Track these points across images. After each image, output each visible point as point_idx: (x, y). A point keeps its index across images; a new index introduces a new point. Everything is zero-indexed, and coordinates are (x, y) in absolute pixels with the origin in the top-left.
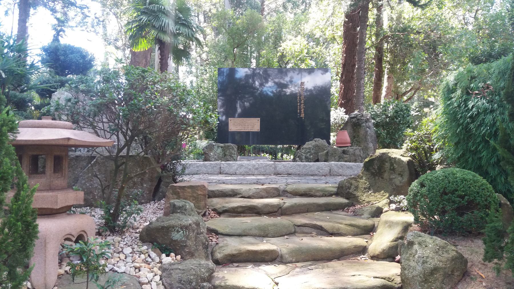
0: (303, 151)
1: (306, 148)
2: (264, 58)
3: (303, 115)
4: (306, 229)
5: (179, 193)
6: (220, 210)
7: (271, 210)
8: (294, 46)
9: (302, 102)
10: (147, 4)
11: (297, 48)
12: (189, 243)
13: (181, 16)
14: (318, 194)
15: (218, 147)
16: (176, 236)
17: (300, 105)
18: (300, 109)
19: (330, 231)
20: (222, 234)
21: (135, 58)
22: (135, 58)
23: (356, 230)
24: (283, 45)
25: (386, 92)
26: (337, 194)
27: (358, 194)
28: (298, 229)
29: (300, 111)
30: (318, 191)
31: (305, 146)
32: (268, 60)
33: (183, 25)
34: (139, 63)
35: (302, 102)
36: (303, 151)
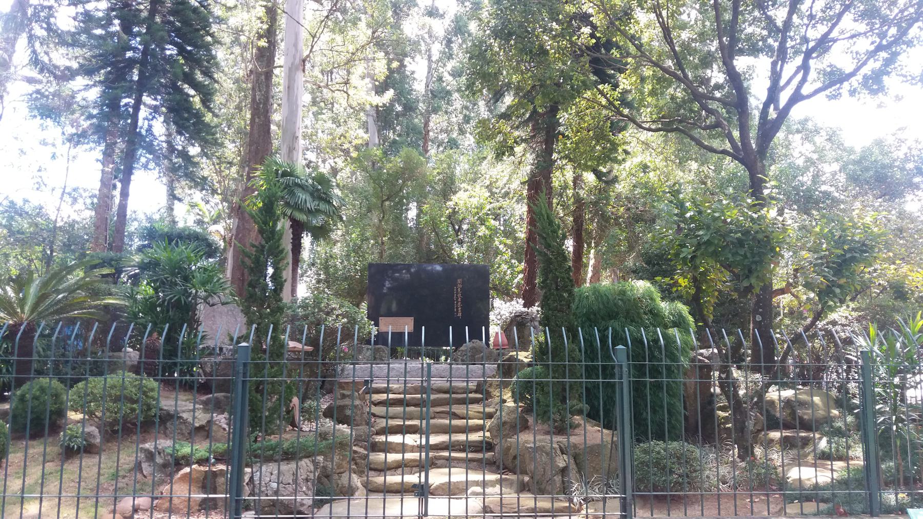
0: (459, 354)
1: (462, 351)
2: (426, 214)
3: (460, 315)
4: (442, 415)
5: (342, 386)
6: (376, 402)
7: (417, 403)
8: (470, 199)
9: (459, 300)
10: (280, 176)
11: (475, 202)
12: (357, 418)
13: (320, 187)
14: (459, 391)
15: (368, 349)
16: (348, 412)
17: (457, 304)
18: (457, 308)
19: (461, 416)
20: (378, 416)
21: (243, 224)
22: (243, 224)
23: (482, 415)
24: (455, 198)
25: (592, 271)
26: (476, 392)
27: (491, 390)
28: (437, 415)
29: (457, 310)
30: (460, 388)
31: (462, 348)
32: (433, 219)
33: (321, 199)
34: (250, 231)
35: (459, 300)
36: (459, 354)
